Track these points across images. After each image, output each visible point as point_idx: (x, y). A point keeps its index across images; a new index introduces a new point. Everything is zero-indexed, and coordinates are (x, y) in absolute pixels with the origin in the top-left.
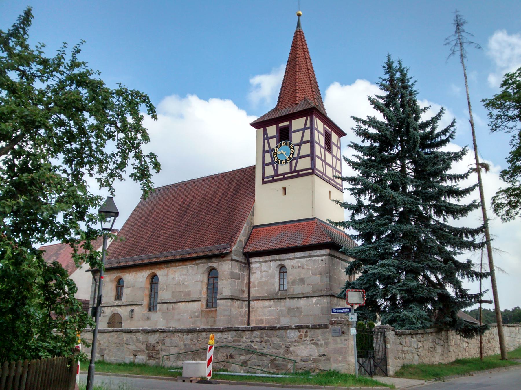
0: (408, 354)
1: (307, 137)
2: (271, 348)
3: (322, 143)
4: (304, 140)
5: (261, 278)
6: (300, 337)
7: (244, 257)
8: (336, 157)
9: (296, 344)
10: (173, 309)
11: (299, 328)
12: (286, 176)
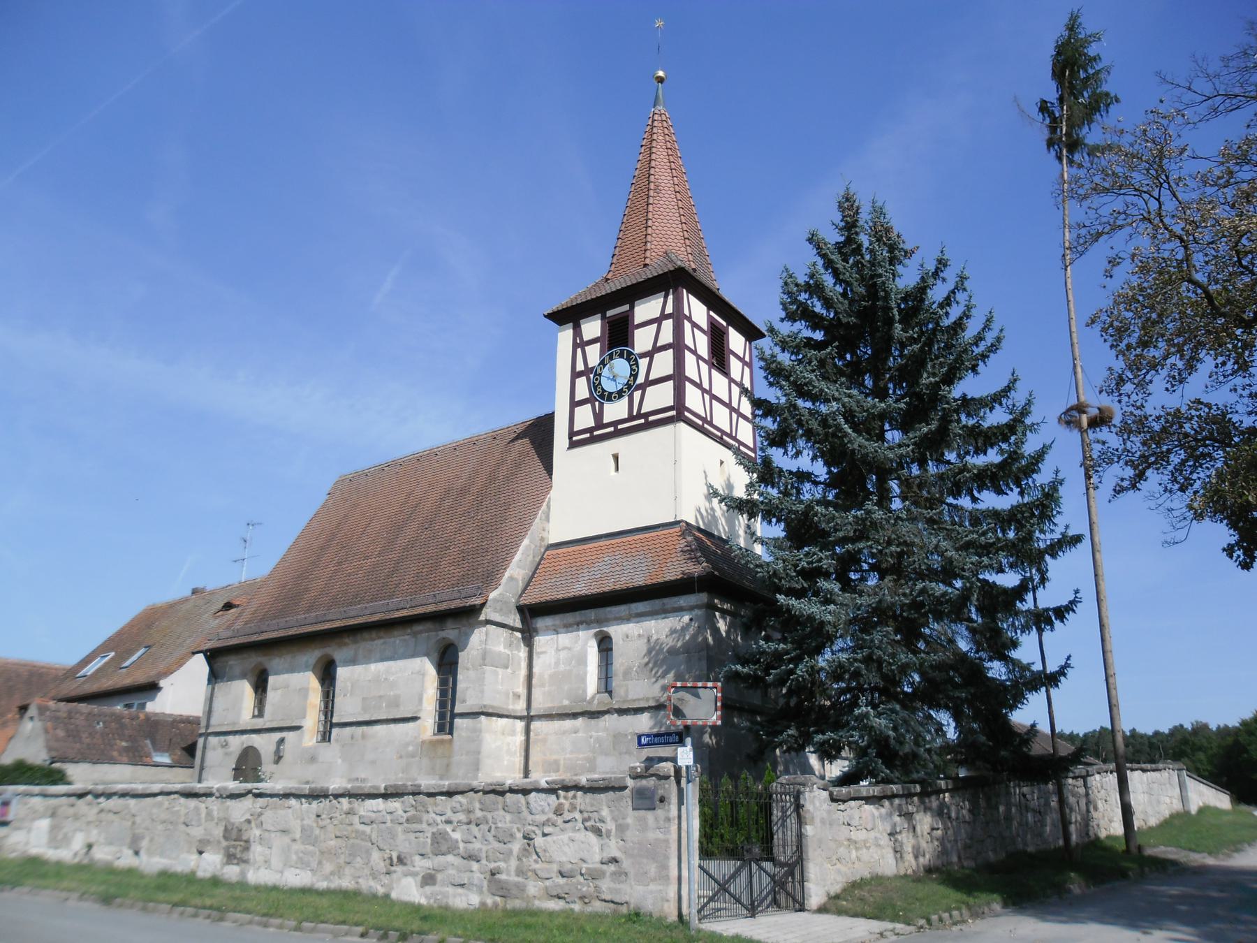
0: (868, 848)
1: (667, 336)
2: (491, 839)
3: (703, 350)
5: (557, 663)
6: (558, 812)
7: (518, 617)
8: (740, 385)
9: (547, 830)
10: (364, 736)
12: (620, 427)
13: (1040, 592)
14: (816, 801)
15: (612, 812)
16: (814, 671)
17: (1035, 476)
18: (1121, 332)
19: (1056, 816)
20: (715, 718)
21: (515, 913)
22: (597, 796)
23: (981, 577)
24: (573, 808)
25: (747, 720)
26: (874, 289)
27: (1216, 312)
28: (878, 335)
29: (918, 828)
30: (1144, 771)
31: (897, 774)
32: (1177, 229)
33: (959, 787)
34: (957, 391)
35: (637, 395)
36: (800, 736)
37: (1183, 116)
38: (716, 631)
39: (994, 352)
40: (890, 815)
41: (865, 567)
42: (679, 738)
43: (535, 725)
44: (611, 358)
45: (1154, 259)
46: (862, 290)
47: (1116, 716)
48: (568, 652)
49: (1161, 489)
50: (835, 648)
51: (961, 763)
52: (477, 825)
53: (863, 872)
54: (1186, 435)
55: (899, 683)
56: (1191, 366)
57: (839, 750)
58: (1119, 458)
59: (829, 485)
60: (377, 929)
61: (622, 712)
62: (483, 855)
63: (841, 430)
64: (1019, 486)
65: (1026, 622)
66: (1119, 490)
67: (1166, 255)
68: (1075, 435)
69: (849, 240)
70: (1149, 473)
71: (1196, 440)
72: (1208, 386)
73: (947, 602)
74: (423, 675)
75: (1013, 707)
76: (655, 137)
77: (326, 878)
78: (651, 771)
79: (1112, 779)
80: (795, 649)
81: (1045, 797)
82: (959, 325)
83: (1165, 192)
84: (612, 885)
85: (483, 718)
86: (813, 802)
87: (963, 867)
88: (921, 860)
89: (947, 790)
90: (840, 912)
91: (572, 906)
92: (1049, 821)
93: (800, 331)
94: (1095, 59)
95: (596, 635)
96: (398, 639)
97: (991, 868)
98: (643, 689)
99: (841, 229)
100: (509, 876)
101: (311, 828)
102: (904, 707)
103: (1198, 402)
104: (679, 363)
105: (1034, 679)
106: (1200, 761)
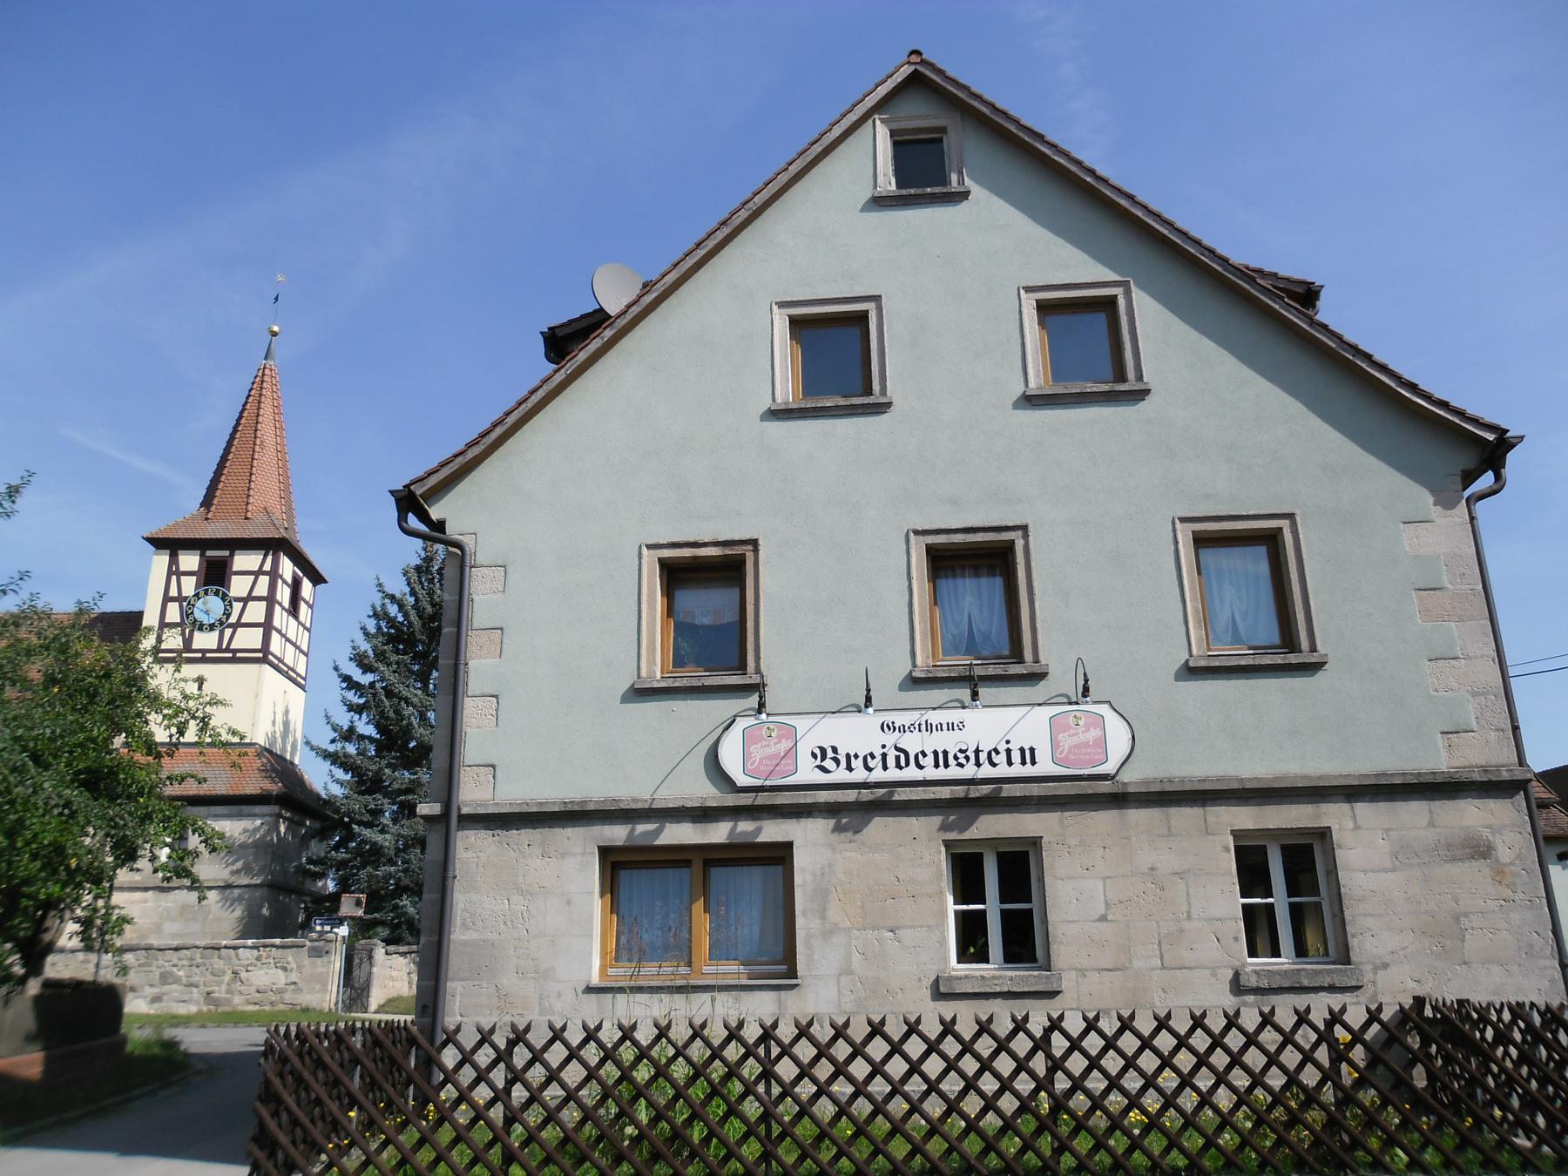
1: (262, 587)
3: (286, 604)
6: (258, 959)
11: (1100, 970)
35: (228, 632)
44: (206, 593)
100: (220, 992)
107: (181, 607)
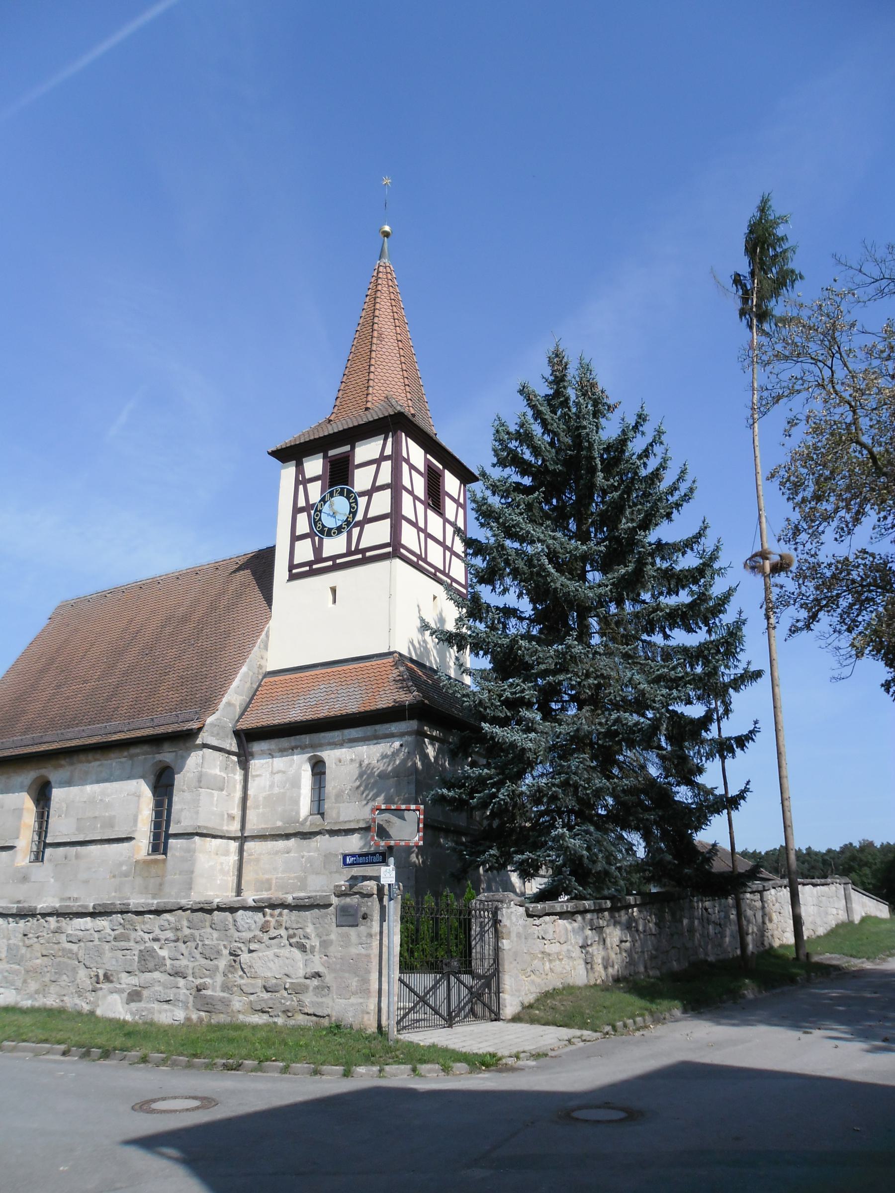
1: (385, 476)
2: (198, 956)
4: (377, 484)
5: (272, 786)
6: (264, 929)
7: (234, 741)
9: (253, 946)
10: (77, 856)
12: (338, 561)
13: (724, 723)
14: (513, 916)
15: (315, 928)
16: (513, 795)
17: (721, 616)
18: (797, 487)
19: (735, 928)
20: (416, 839)
21: (220, 1027)
22: (302, 913)
23: (671, 708)
24: (279, 925)
25: (453, 841)
26: (579, 440)
27: (879, 472)
28: (582, 482)
29: (608, 941)
30: (814, 885)
31: (590, 891)
32: (846, 395)
33: (648, 901)
34: (652, 536)
36: (501, 856)
37: (854, 294)
38: (424, 756)
39: (688, 501)
40: (582, 929)
41: (566, 698)
42: (382, 857)
43: (248, 845)
44: (332, 496)
45: (826, 421)
46: (569, 440)
47: (790, 837)
48: (282, 775)
49: (831, 630)
50: (535, 773)
51: (648, 880)
52: (185, 943)
53: (556, 982)
54: (853, 581)
55: (593, 807)
56: (857, 520)
57: (537, 868)
58: (795, 601)
59: (532, 621)
60: (80, 1046)
61: (333, 833)
62: (190, 972)
63: (545, 570)
64: (707, 624)
65: (711, 750)
66: (794, 630)
67: (836, 418)
68: (759, 580)
69: (558, 393)
70: (821, 615)
71: (861, 586)
72: (869, 538)
73: (639, 730)
74: (139, 796)
75: (697, 828)
76: (379, 287)
77: (31, 997)
78: (355, 890)
79: (786, 893)
80: (498, 774)
81: (725, 911)
82: (656, 476)
83: (837, 362)
84: (315, 999)
85: (197, 838)
86: (509, 918)
87: (649, 976)
88: (610, 970)
89: (635, 905)
90: (533, 1021)
91: (276, 1020)
92: (728, 932)
93: (509, 477)
94: (783, 239)
95: (310, 759)
96: (114, 761)
97: (675, 977)
98: (353, 811)
99: (550, 383)
100: (214, 992)
101: (18, 947)
102: (598, 828)
103: (864, 552)
104: (396, 502)
105: (716, 803)
106: (865, 875)
107: (309, 516)
